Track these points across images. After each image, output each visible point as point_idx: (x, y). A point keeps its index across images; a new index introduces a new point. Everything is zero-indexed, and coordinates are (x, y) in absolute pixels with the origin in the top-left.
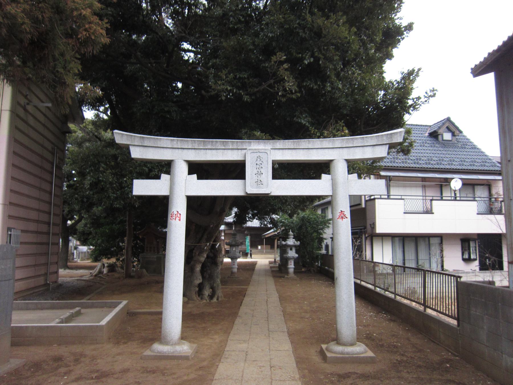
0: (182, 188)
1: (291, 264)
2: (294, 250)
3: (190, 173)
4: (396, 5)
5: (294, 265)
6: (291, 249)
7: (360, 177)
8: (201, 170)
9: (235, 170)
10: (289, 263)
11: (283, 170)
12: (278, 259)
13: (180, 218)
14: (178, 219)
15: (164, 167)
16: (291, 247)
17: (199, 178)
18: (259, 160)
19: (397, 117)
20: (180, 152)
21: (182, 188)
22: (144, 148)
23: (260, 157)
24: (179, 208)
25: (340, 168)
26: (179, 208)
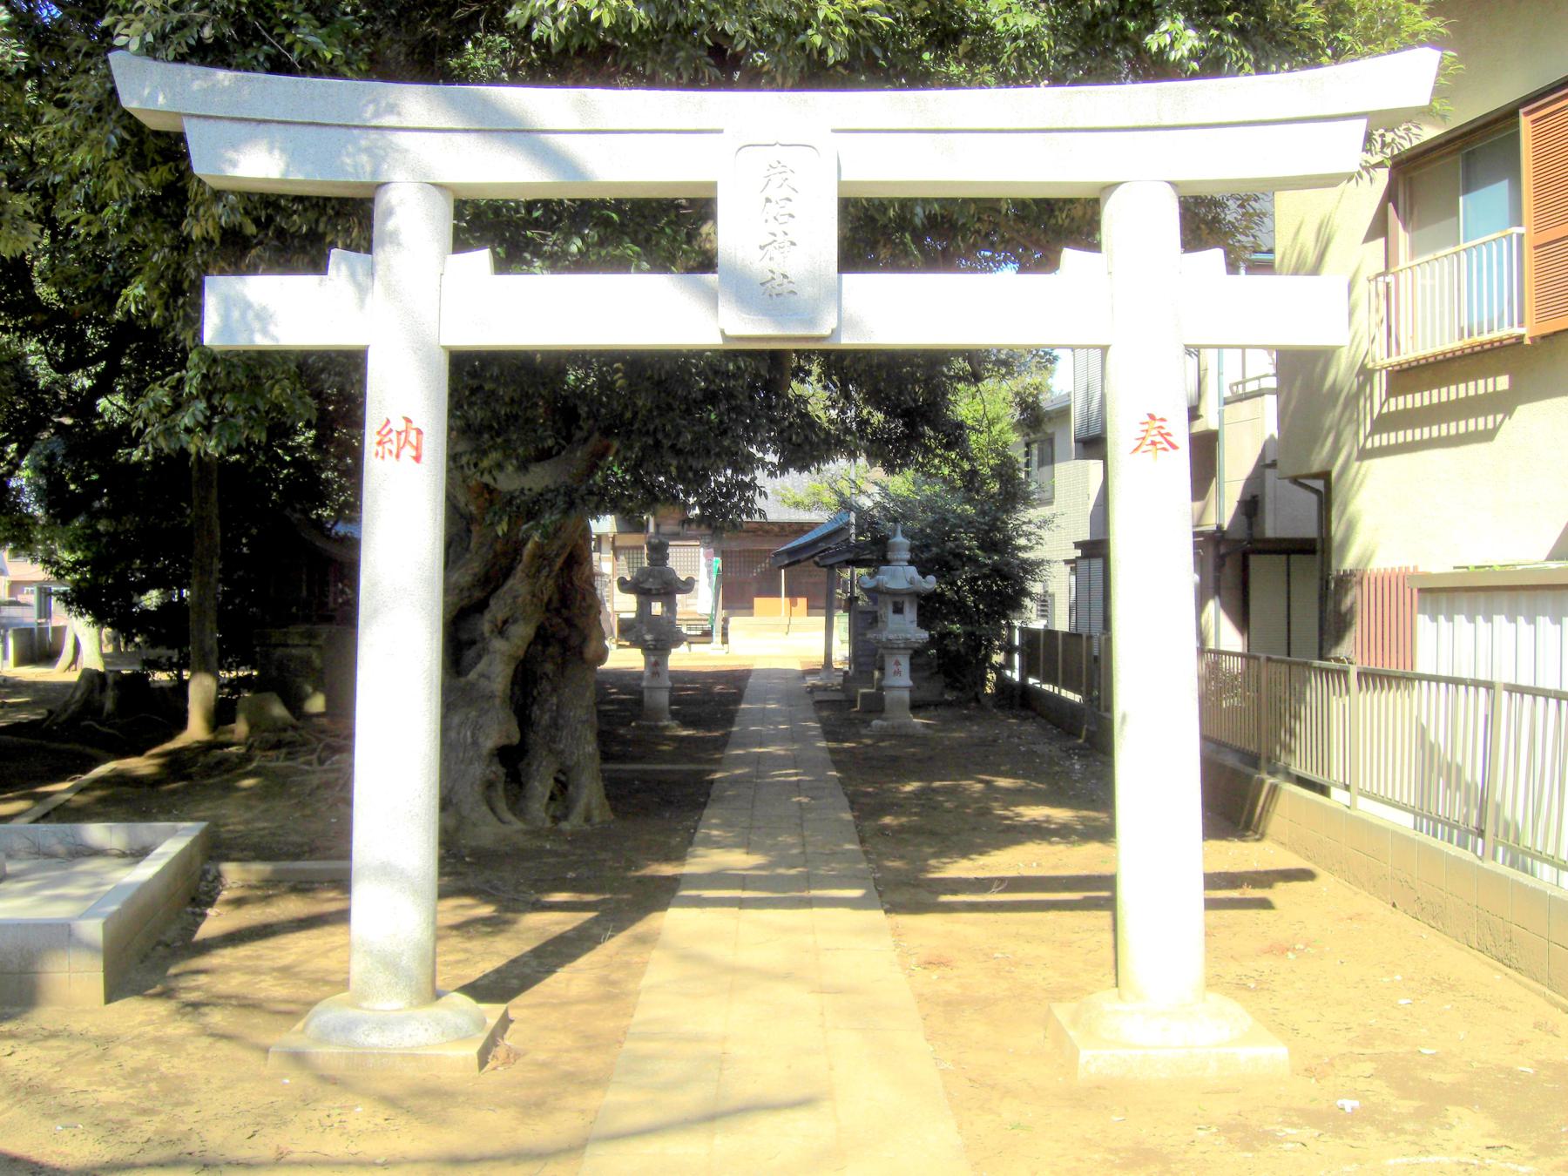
0: (402, 317)
1: (898, 673)
2: (911, 614)
3: (461, 243)
4: (1023, 475)
5: (912, 678)
6: (898, 610)
7: (1232, 268)
8: (503, 229)
9: (663, 230)
10: (890, 667)
11: (882, 231)
12: (842, 651)
13: (417, 448)
14: (408, 452)
15: (313, 227)
16: (898, 602)
17: (503, 265)
18: (777, 180)
19: (484, 453)
20: (425, 144)
21: (402, 317)
22: (250, 137)
23: (775, 168)
24: (405, 414)
25: (1140, 223)
26: (405, 414)
